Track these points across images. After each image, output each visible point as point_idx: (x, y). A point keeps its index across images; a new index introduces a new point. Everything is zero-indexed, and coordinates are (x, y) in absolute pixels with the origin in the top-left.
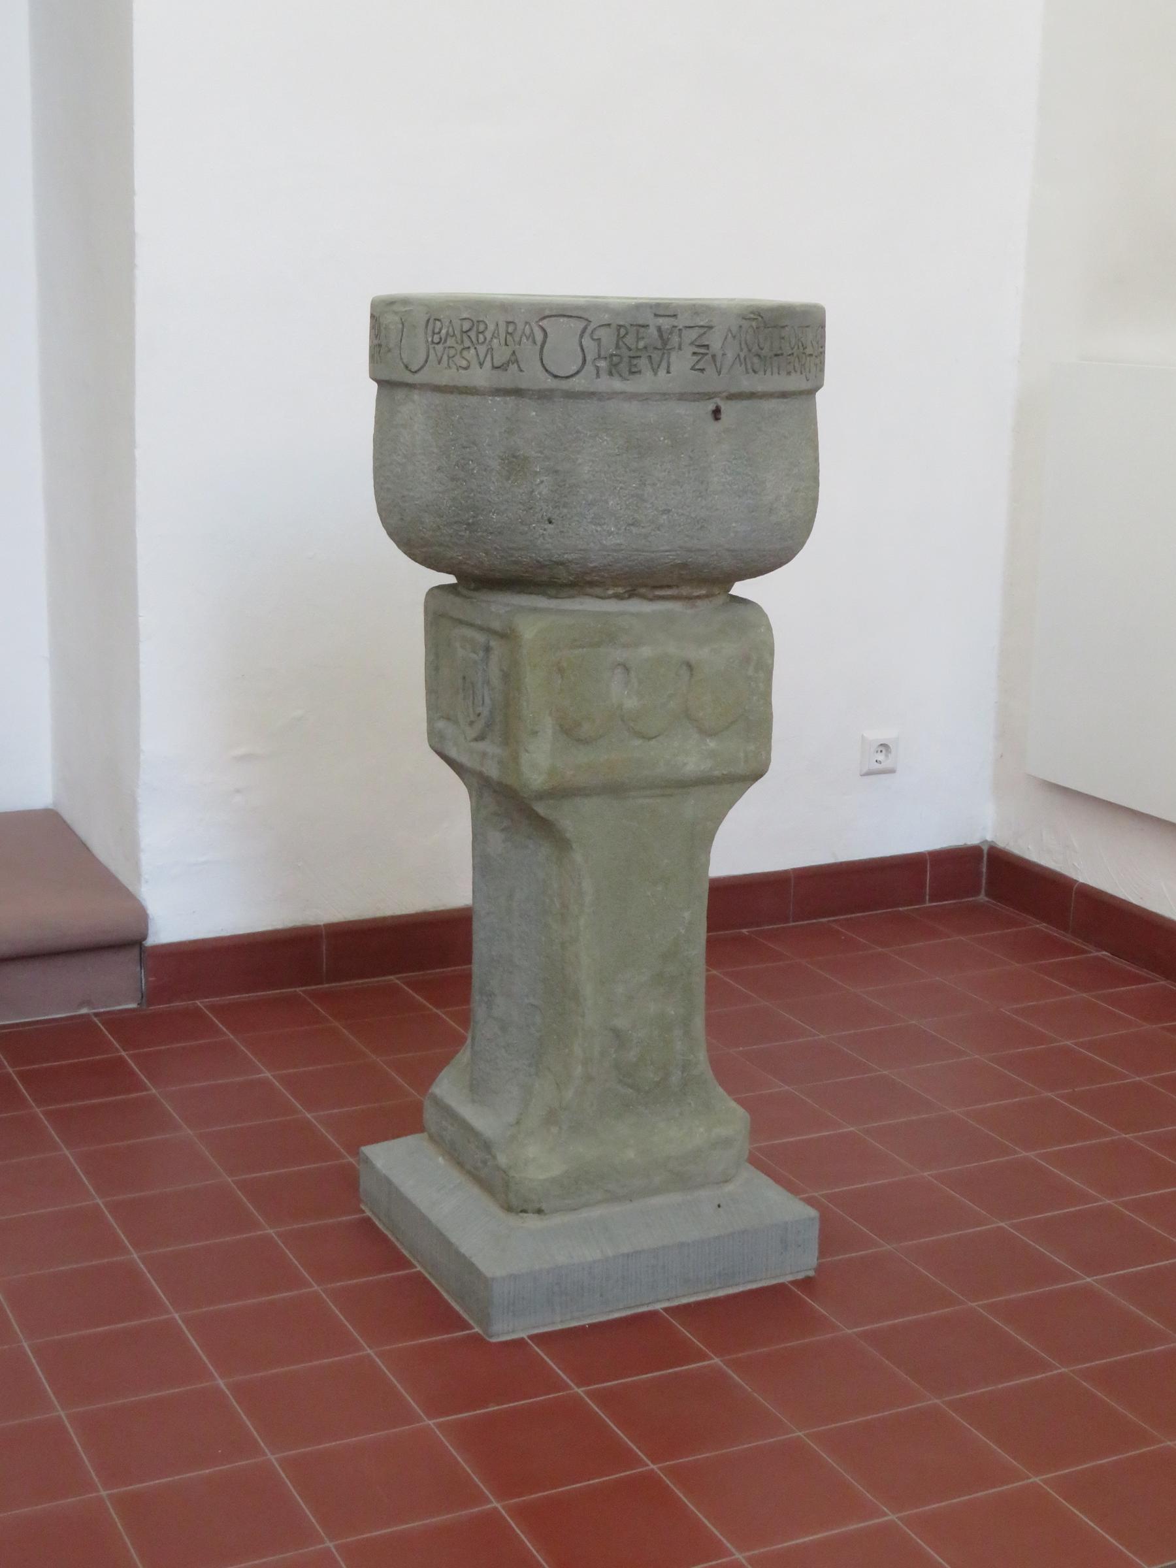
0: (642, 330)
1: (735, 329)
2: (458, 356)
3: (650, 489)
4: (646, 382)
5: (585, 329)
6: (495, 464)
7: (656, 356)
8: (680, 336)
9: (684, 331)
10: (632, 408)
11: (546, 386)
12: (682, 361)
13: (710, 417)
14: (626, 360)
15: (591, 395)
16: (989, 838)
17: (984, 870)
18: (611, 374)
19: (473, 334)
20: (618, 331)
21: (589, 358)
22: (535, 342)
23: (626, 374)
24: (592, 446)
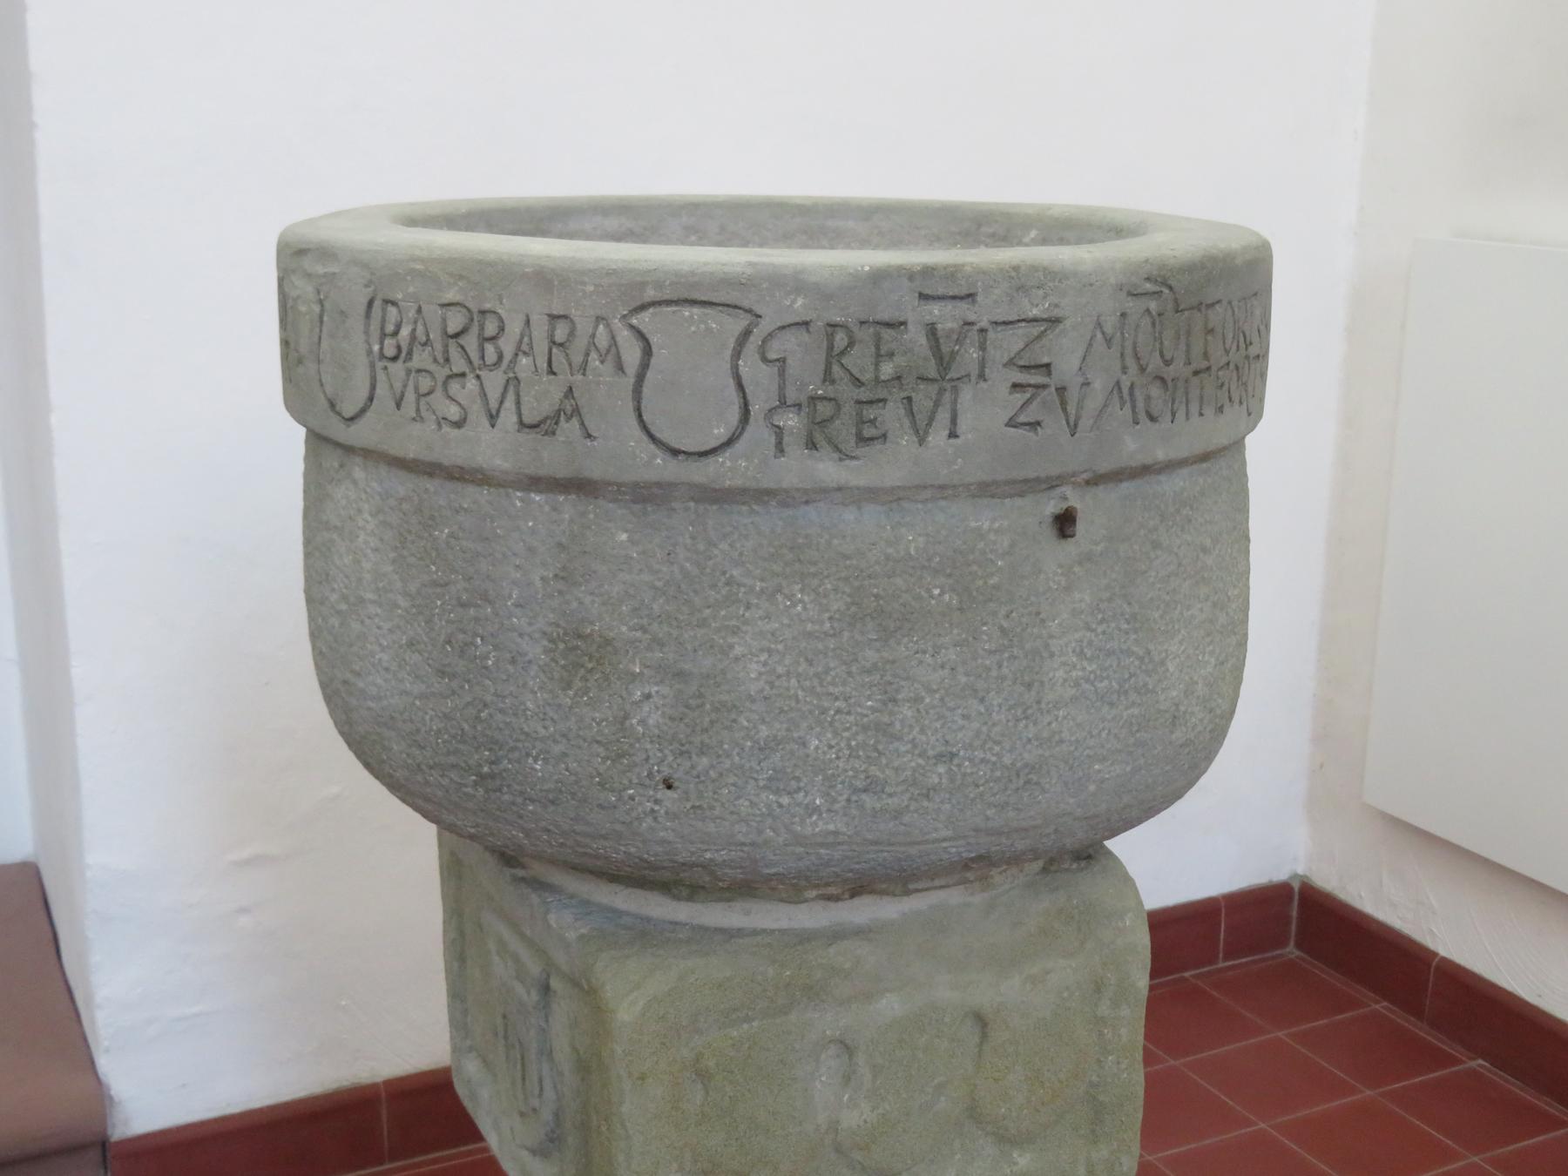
0: (887, 334)
1: (1110, 325)
2: (439, 393)
3: (907, 712)
4: (893, 463)
5: (747, 333)
6: (535, 650)
7: (923, 398)
8: (982, 347)
9: (991, 335)
10: (865, 523)
11: (650, 475)
12: (984, 411)
13: (1049, 532)
14: (848, 409)
15: (762, 496)
16: (1300, 871)
17: (1294, 913)
18: (812, 445)
19: (470, 341)
20: (830, 338)
21: (755, 408)
22: (620, 367)
23: (849, 444)
24: (768, 617)
